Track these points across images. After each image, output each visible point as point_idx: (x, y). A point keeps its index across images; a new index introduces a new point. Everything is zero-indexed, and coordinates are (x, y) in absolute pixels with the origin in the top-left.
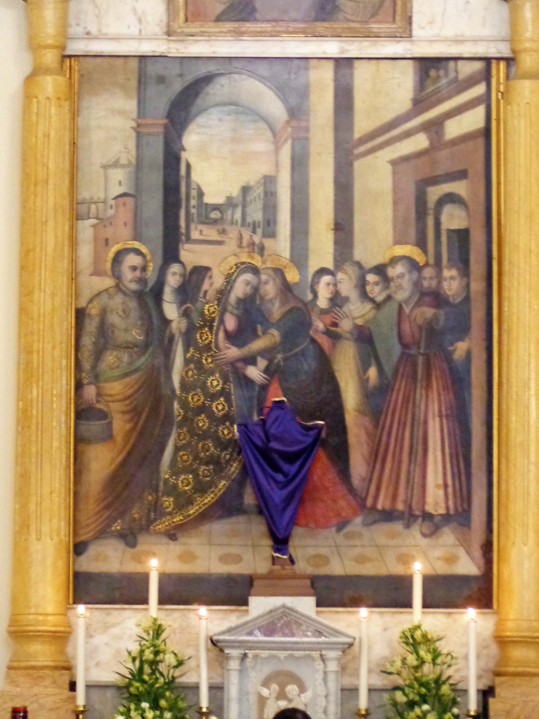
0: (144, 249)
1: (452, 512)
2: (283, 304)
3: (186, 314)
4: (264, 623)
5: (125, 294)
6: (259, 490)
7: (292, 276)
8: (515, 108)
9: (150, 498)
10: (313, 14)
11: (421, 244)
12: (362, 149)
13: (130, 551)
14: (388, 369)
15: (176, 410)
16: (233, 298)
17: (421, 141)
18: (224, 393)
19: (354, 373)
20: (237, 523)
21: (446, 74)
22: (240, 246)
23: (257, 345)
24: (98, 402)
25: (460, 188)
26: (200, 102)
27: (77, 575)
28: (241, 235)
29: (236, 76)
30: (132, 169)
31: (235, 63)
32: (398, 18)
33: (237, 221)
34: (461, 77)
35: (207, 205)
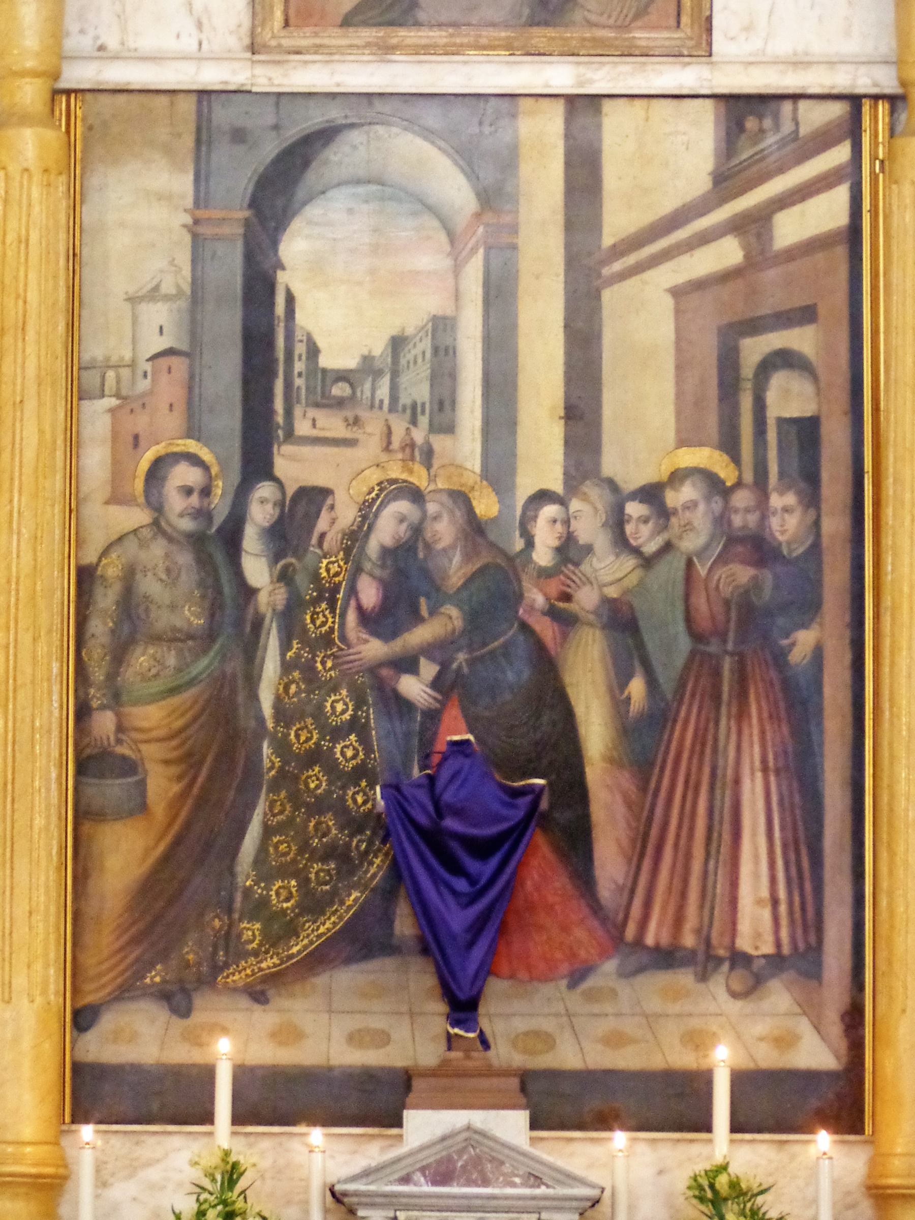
0: (206, 455)
1: (786, 950)
2: (468, 558)
3: (285, 577)
5: (170, 539)
6: (424, 912)
7: (486, 505)
9: (217, 923)
10: (526, 11)
11: (729, 444)
12: (617, 266)
13: (179, 1024)
14: (667, 680)
16: (373, 547)
17: (728, 253)
18: (356, 726)
19: (602, 689)
20: (380, 970)
21: (777, 126)
22: (387, 448)
23: (420, 635)
24: (119, 741)
25: (801, 340)
26: (311, 177)
27: (78, 1068)
28: (389, 428)
29: (380, 129)
30: (183, 304)
31: (378, 105)
32: (685, 19)
33: (381, 401)
35: (324, 371)
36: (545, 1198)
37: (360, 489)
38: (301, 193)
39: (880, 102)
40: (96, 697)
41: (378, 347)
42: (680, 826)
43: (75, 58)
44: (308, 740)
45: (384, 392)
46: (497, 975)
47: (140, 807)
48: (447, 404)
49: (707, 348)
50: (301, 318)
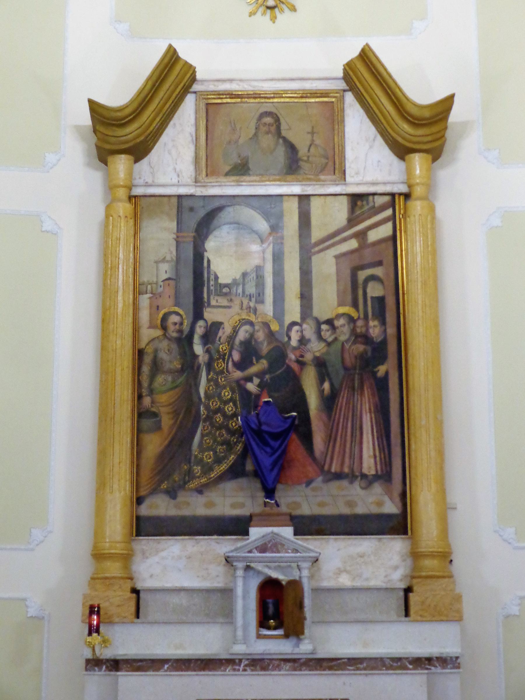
0: (181, 312)
1: (379, 473)
2: (269, 344)
3: (208, 351)
4: (259, 544)
5: (169, 339)
6: (257, 461)
7: (275, 327)
8: (412, 218)
9: (186, 467)
10: (285, 171)
11: (355, 305)
12: (316, 249)
13: (173, 501)
15: (202, 412)
16: (237, 341)
17: (353, 244)
18: (231, 400)
19: (315, 385)
20: (243, 481)
21: (368, 204)
22: (242, 308)
23: (253, 370)
24: (152, 407)
25: (378, 271)
26: (215, 222)
27: (138, 518)
28: (242, 302)
29: (238, 207)
30: (173, 263)
31: (237, 199)
32: (336, 172)
33: (239, 294)
34: (377, 205)
35: (220, 284)
36: (300, 557)
37: (232, 322)
38: (212, 227)
39: (401, 196)
40: (145, 392)
41: (238, 276)
42: (342, 432)
43: (137, 186)
44: (216, 405)
45: (240, 290)
46: (281, 483)
47: (158, 427)
48: (261, 294)
49: (347, 273)
50: (212, 267)
